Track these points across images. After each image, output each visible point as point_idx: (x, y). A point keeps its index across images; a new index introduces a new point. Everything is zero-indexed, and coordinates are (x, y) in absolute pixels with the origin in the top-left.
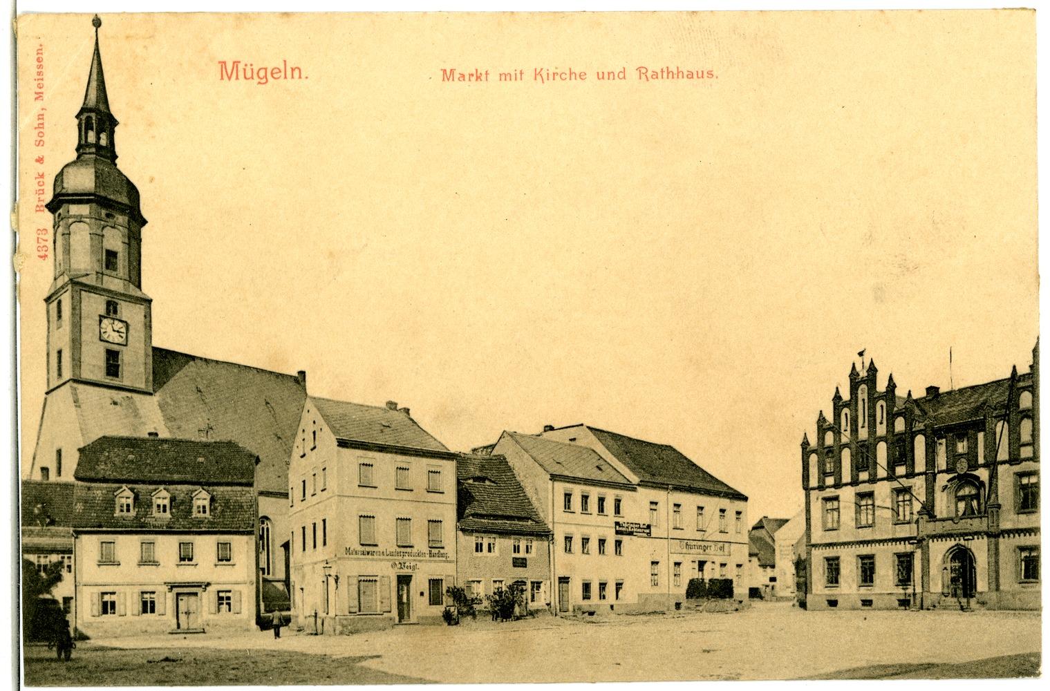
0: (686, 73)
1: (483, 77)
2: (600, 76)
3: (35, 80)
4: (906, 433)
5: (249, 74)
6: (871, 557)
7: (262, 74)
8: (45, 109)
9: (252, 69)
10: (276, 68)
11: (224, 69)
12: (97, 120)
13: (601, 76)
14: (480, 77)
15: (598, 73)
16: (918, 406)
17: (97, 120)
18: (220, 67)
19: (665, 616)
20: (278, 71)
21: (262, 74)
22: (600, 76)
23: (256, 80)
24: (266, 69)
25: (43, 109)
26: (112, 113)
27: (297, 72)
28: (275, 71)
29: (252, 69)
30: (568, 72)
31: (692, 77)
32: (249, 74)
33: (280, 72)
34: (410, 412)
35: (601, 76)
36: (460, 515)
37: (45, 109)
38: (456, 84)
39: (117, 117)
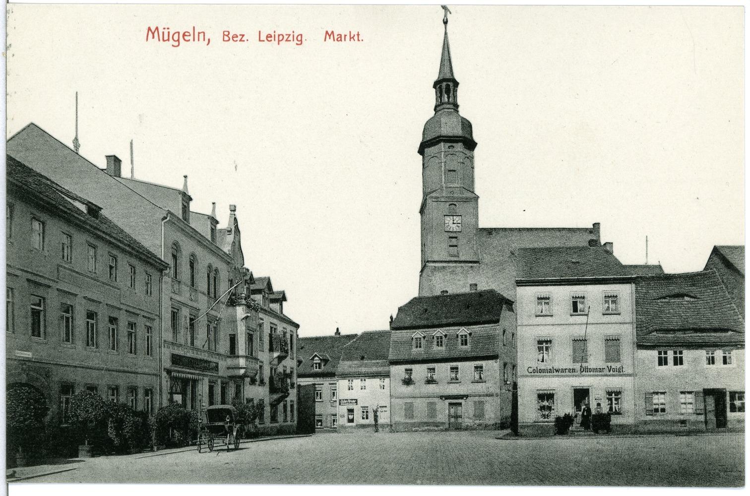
1: (356, 38)
3: (275, 32)
4: (281, 344)
5: (166, 38)
6: (411, 370)
7: (176, 37)
9: (169, 32)
10: (270, 35)
12: (446, 87)
14: (353, 38)
17: (446, 87)
19: (537, 389)
21: (176, 37)
23: (296, 41)
24: (179, 33)
25: (209, 40)
26: (359, 333)
27: (201, 36)
28: (269, 36)
29: (169, 32)
31: (341, 40)
32: (166, 38)
33: (190, 35)
36: (525, 249)
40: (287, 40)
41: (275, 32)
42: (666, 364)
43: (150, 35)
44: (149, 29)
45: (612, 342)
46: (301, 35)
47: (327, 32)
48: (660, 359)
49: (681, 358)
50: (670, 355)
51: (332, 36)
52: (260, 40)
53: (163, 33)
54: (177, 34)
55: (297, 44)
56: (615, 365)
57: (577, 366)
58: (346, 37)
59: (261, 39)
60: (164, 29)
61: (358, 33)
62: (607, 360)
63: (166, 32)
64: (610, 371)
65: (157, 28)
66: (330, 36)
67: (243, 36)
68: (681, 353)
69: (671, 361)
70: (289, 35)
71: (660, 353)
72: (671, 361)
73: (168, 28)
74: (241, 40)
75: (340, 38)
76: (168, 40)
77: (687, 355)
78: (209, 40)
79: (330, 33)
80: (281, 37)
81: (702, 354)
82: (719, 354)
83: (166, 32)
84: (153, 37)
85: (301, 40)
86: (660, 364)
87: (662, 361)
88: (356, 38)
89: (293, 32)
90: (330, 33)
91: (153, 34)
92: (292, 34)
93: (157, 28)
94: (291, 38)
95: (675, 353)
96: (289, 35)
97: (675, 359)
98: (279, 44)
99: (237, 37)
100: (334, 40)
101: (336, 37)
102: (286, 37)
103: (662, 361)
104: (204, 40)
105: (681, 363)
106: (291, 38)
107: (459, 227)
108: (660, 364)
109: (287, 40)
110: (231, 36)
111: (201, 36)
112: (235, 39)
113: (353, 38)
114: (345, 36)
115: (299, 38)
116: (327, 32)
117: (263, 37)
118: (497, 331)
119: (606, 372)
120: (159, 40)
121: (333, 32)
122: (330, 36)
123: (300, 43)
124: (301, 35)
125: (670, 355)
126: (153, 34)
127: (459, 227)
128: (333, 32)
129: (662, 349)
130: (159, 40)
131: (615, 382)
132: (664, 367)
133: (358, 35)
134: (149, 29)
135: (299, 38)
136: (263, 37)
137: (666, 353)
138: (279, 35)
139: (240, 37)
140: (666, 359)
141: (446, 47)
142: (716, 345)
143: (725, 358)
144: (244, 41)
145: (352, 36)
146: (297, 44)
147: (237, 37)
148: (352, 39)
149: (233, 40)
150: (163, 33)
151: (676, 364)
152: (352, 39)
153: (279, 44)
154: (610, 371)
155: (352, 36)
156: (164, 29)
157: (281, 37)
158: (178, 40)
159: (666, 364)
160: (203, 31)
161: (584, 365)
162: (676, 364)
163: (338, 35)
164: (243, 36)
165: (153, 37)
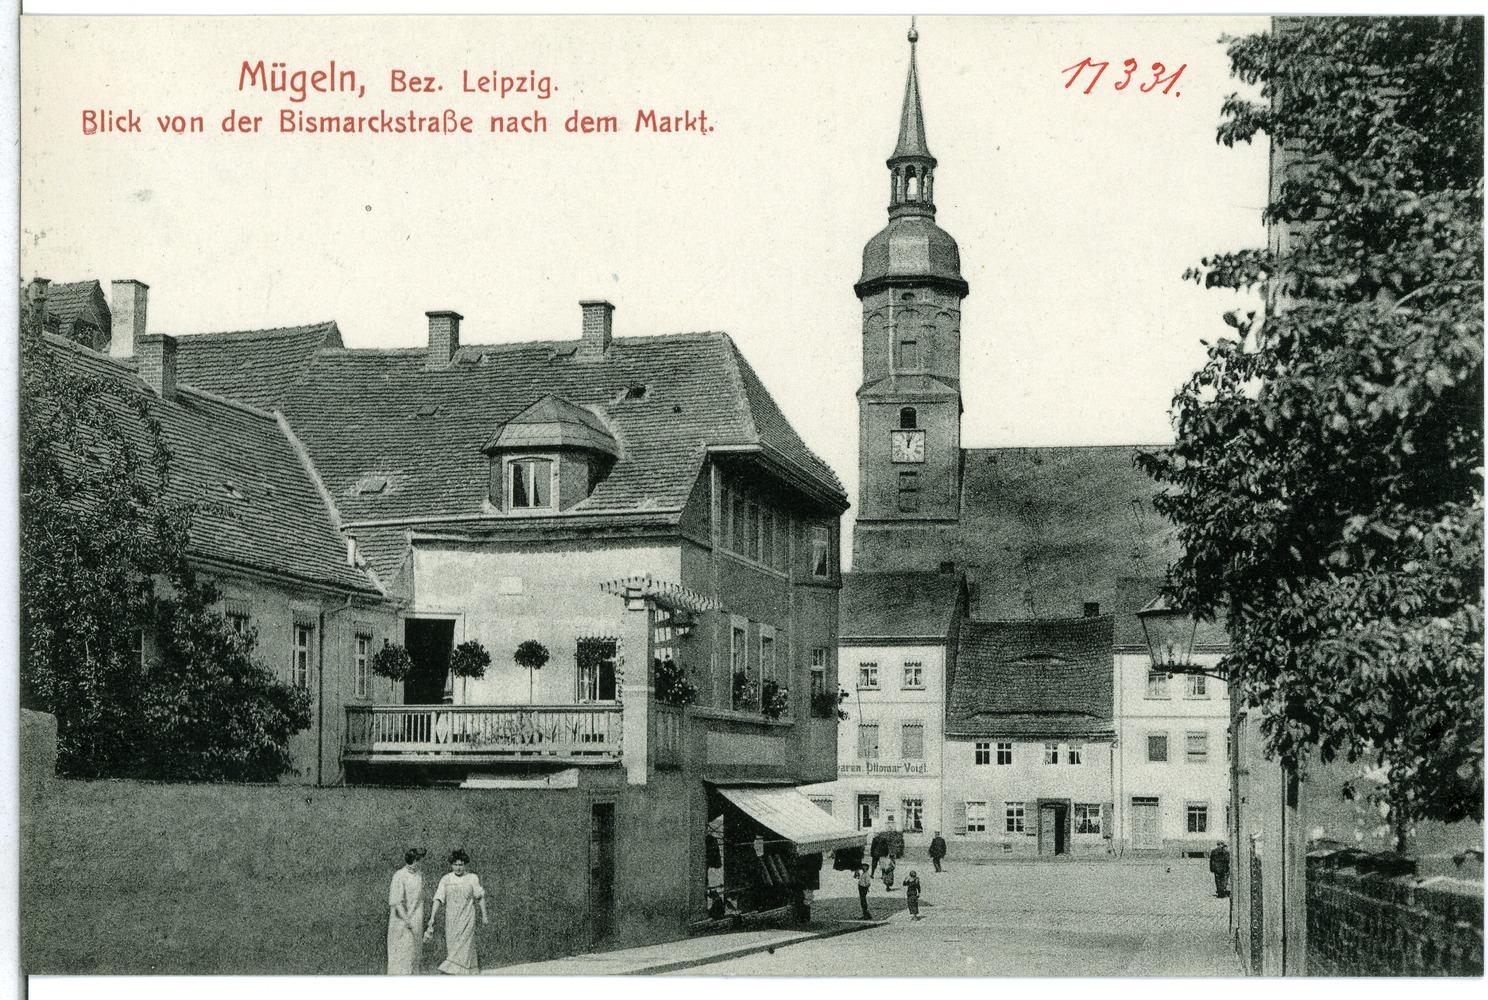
0: (342, 123)
1: (698, 124)
2: (610, 123)
3: (495, 73)
5: (279, 83)
7: (298, 83)
8: (361, 96)
9: (284, 73)
11: (913, 85)
13: (197, 123)
15: (545, 130)
16: (1048, 634)
18: (1269, 142)
20: (300, 77)
21: (298, 83)
22: (610, 123)
23: (537, 91)
24: (304, 74)
25: (363, 88)
27: (348, 79)
28: (318, 76)
29: (284, 73)
30: (533, 116)
32: (279, 83)
34: (615, 314)
35: (197, 123)
37: (361, 96)
38: (300, 137)
39: (313, 318)
40: (519, 90)
41: (495, 73)
42: (987, 761)
43: (248, 78)
44: (246, 65)
45: (912, 727)
46: (548, 79)
47: (641, 114)
48: (979, 755)
49: (1009, 755)
50: (994, 749)
51: (650, 122)
52: (466, 90)
53: (273, 73)
54: (300, 77)
55: (540, 97)
56: (915, 763)
57: (863, 763)
58: (680, 122)
59: (468, 88)
60: (275, 65)
61: (703, 112)
62: (905, 754)
63: (279, 71)
64: (907, 770)
65: (261, 65)
66: (646, 121)
67: (431, 80)
68: (1009, 746)
69: (994, 758)
70: (524, 80)
71: (979, 746)
72: (994, 758)
73: (283, 65)
74: (427, 89)
75: (666, 126)
76: (283, 88)
77: (1018, 749)
78: (363, 88)
79: (646, 116)
80: (507, 84)
81: (1039, 749)
82: (1063, 749)
83: (279, 71)
84: (254, 83)
85: (548, 90)
86: (979, 761)
87: (982, 758)
88: (698, 124)
89: (533, 73)
90: (646, 116)
91: (253, 76)
92: (529, 76)
93: (261, 65)
94: (527, 85)
95: (1000, 746)
96: (524, 80)
97: (1000, 755)
98: (503, 96)
99: (419, 82)
100: (655, 130)
101: (659, 123)
102: (517, 83)
103: (982, 758)
104: (353, 89)
105: (1009, 761)
106: (527, 85)
107: (919, 452)
108: (979, 761)
109: (519, 90)
110: (407, 80)
111: (348, 79)
112: (416, 87)
113: (692, 124)
114: (678, 120)
115: (544, 85)
116: (641, 114)
117: (473, 83)
118: (1379, 774)
119: (902, 771)
120: (265, 88)
121: (652, 113)
122: (646, 121)
123: (545, 94)
124: (548, 79)
125: (994, 749)
126: (253, 76)
127: (919, 452)
128: (652, 113)
129: (1006, 741)
130: (265, 88)
131: (913, 787)
132: (983, 767)
133: (703, 118)
134: (246, 65)
135: (544, 85)
136: (473, 83)
137: (987, 746)
138: (503, 80)
139: (424, 84)
140: (987, 754)
141: (912, 164)
142: (1062, 736)
143: (1072, 754)
144: (433, 90)
145: (691, 120)
146: (540, 97)
147: (419, 82)
148: (690, 128)
149: (412, 89)
150: (273, 73)
151: (1001, 762)
152: (690, 128)
153: (503, 96)
154: (907, 770)
155: (691, 120)
156: (275, 65)
157: (507, 84)
158: (303, 89)
159: (987, 761)
160: (350, 69)
161: (873, 761)
162: (1001, 762)
163: (663, 119)
164: (431, 80)
165: (254, 83)
